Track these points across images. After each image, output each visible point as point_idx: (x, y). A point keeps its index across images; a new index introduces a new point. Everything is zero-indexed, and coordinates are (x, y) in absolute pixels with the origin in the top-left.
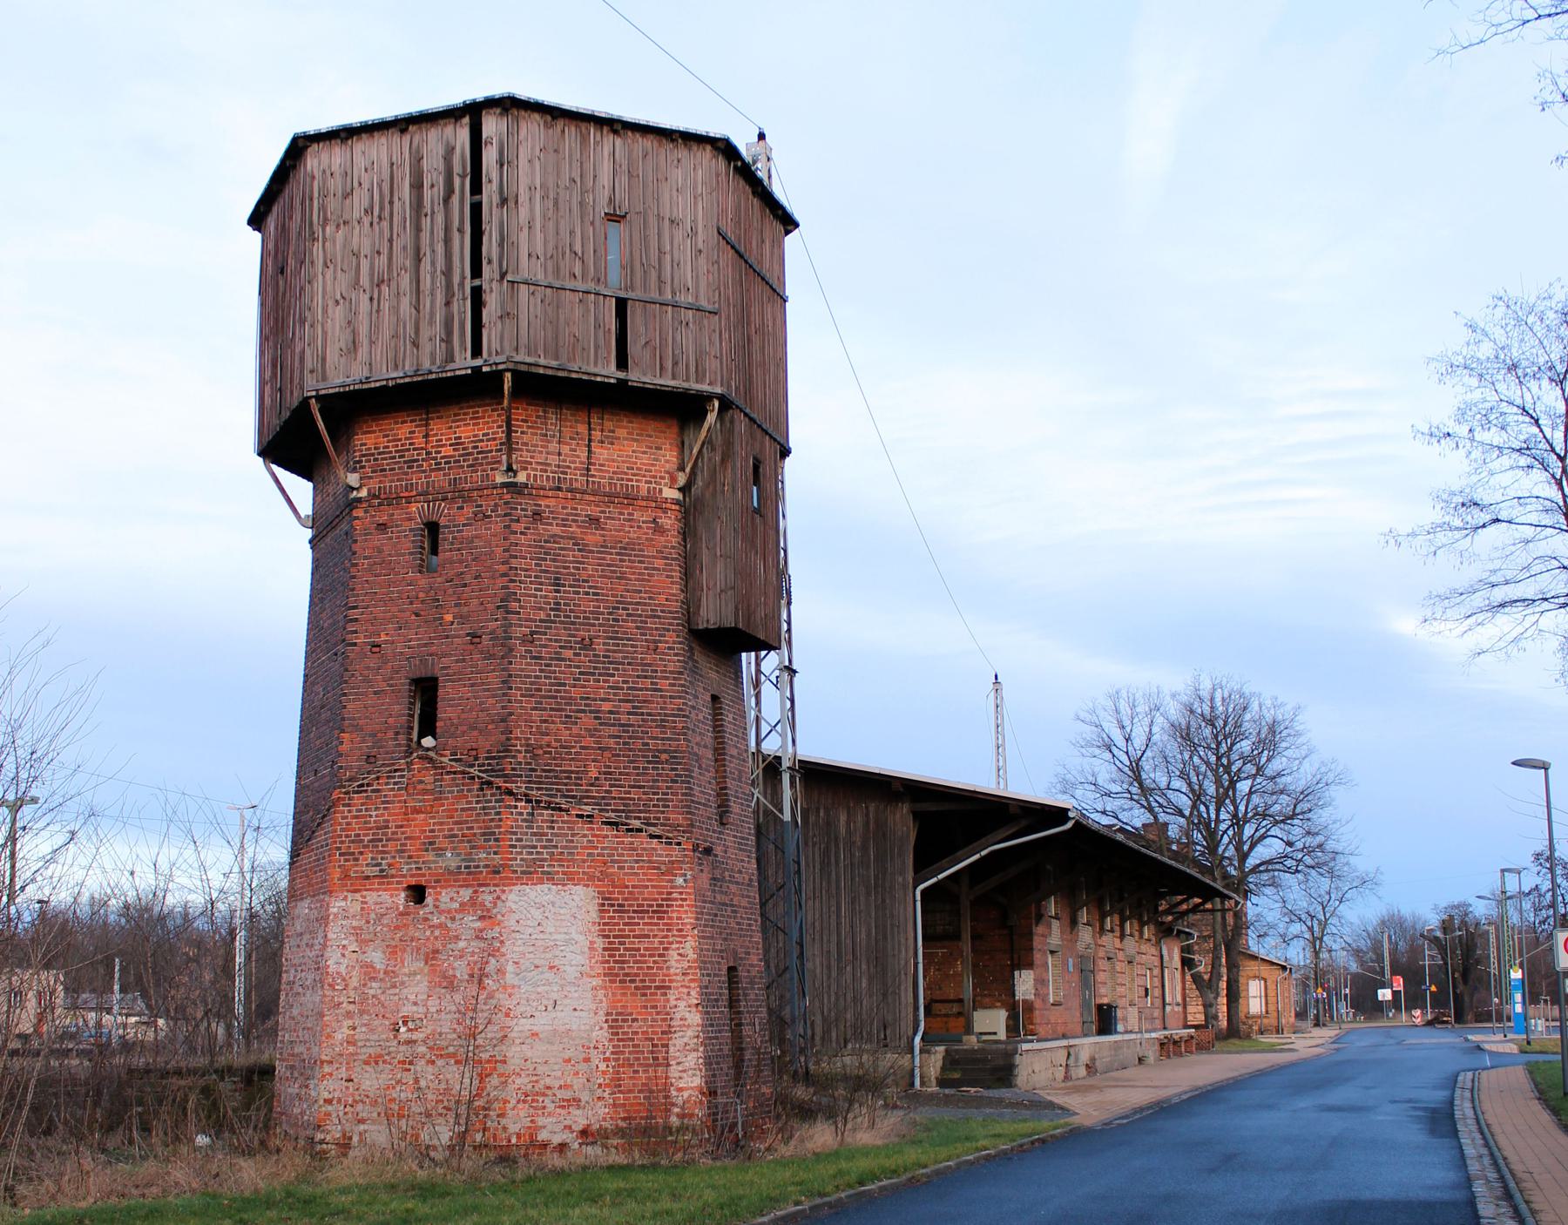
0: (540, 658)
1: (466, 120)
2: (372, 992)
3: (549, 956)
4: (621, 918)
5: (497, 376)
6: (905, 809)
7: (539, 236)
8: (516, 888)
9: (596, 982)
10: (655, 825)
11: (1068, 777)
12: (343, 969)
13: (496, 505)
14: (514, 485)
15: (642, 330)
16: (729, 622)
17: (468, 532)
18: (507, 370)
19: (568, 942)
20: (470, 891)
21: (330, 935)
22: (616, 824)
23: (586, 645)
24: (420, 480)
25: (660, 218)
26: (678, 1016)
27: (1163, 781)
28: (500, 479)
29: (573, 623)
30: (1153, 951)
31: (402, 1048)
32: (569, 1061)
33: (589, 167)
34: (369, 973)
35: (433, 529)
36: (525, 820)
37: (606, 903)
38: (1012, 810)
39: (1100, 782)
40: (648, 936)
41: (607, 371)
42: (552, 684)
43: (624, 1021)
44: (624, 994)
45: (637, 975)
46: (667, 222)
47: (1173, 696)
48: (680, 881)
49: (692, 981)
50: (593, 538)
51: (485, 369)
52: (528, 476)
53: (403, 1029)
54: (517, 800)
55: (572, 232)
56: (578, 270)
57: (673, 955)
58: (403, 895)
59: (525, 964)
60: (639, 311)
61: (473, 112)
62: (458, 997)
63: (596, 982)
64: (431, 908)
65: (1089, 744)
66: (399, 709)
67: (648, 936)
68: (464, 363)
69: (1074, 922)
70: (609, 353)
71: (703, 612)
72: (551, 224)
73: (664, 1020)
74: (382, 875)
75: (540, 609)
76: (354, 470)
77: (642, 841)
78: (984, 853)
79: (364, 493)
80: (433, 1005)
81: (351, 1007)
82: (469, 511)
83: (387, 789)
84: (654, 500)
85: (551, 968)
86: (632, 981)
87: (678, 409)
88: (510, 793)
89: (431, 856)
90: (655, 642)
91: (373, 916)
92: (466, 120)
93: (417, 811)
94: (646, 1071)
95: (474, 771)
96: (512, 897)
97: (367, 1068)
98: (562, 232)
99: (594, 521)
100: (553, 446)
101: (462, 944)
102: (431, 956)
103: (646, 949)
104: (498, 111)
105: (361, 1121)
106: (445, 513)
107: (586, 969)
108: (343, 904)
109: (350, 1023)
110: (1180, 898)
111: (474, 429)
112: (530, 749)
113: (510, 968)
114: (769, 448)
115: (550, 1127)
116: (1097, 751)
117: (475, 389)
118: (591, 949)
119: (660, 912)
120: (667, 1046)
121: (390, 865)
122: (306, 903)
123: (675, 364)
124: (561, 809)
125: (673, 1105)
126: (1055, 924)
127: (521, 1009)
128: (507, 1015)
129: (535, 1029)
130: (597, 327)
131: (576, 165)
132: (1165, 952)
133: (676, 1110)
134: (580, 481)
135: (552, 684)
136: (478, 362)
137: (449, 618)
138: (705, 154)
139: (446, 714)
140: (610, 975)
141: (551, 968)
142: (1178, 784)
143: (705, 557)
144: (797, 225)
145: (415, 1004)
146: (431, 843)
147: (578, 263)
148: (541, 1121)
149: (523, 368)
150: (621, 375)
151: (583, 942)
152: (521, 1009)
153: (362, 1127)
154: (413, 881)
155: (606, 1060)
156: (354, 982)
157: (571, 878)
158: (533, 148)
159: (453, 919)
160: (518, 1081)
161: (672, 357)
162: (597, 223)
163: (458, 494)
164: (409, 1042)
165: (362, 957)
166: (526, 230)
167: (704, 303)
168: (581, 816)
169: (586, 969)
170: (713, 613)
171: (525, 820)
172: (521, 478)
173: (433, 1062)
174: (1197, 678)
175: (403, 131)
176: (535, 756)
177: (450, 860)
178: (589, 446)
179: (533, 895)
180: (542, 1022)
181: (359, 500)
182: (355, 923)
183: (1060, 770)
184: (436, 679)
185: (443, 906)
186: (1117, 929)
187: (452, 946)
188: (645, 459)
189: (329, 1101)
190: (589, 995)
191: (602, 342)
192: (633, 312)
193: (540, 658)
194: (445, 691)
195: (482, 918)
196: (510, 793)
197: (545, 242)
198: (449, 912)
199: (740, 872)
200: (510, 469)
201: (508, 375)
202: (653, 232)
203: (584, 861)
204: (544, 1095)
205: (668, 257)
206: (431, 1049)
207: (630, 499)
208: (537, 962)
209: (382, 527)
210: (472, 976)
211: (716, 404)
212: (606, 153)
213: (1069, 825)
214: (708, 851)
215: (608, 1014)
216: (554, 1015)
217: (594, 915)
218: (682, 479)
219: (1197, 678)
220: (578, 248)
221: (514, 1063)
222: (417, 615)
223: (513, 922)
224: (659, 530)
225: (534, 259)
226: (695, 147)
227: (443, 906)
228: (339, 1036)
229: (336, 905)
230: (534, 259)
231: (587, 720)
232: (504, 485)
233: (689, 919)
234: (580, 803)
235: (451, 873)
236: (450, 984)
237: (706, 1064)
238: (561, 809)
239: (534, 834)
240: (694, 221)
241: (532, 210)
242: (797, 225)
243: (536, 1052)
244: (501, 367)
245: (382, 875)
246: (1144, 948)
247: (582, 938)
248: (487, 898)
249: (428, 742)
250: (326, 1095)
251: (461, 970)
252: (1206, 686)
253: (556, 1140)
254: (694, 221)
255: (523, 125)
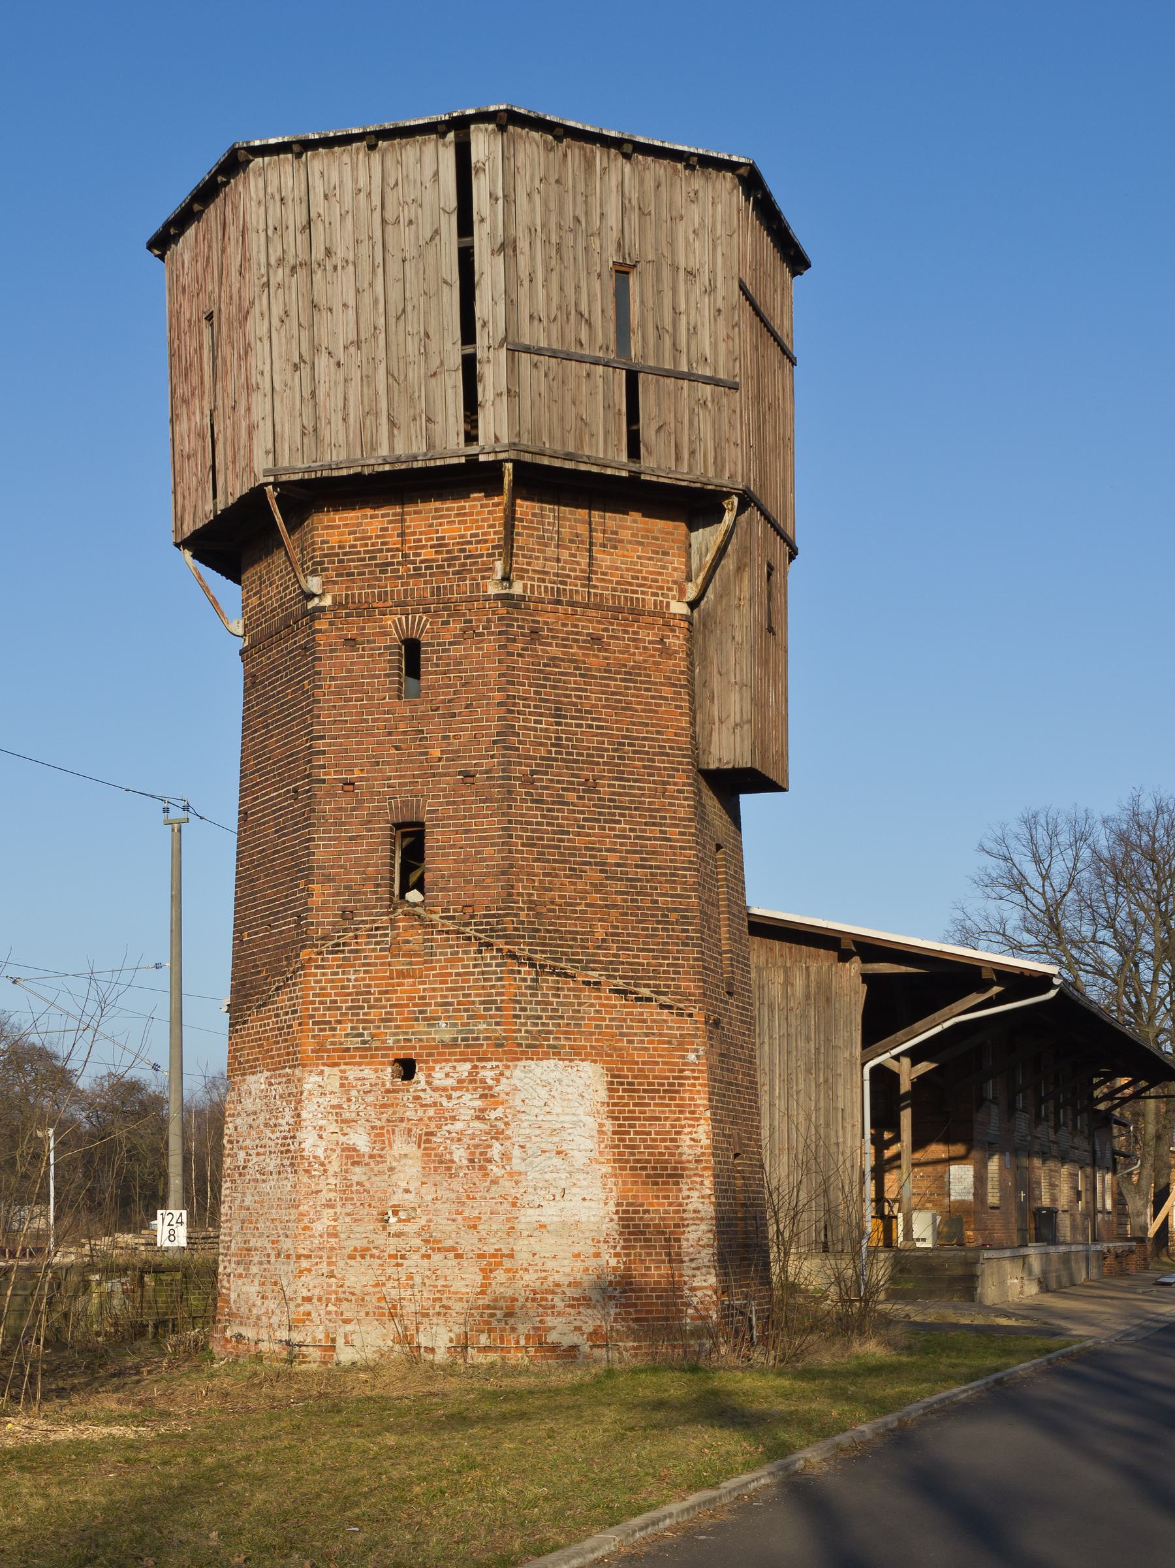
0: (542, 802)
1: (451, 136)
2: (355, 1179)
3: (556, 1139)
4: (632, 1098)
5: (497, 466)
6: (855, 967)
7: (541, 292)
8: (523, 1063)
9: (606, 1169)
10: (665, 994)
11: (968, 923)
12: (320, 1153)
13: (489, 620)
14: (510, 597)
15: (654, 411)
16: (745, 762)
17: (457, 652)
18: (507, 461)
19: (575, 1124)
20: (467, 1066)
21: (304, 1115)
22: (624, 992)
23: (591, 787)
24: (395, 588)
25: (675, 268)
26: (691, 1207)
27: (1087, 930)
28: (493, 590)
29: (576, 761)
30: (1085, 1145)
31: (392, 1241)
32: (578, 1255)
33: (595, 202)
34: (351, 1155)
35: (412, 652)
36: (528, 987)
37: (615, 1080)
38: (985, 975)
39: (1009, 932)
40: (659, 1119)
41: (617, 462)
42: (554, 832)
43: (635, 1212)
44: (635, 1183)
45: (648, 1162)
46: (682, 273)
47: (1105, 822)
48: (692, 1057)
49: (705, 1169)
50: (595, 661)
51: (482, 458)
52: (525, 586)
53: (393, 1220)
54: (520, 964)
55: (577, 288)
56: (584, 338)
57: (686, 1140)
58: (389, 1070)
59: (532, 1148)
60: (652, 388)
61: (461, 125)
62: (456, 1184)
63: (606, 1169)
64: (423, 1085)
65: (993, 883)
66: (379, 855)
67: (659, 1119)
68: (451, 447)
69: (1012, 1108)
70: (619, 440)
71: (714, 749)
72: (555, 277)
73: (678, 1212)
74: (365, 1048)
75: (541, 744)
76: (314, 573)
77: (650, 1012)
78: (947, 1025)
79: (327, 601)
80: (428, 1194)
81: (332, 1195)
82: (456, 627)
83: (369, 949)
84: (660, 613)
85: (558, 1153)
86: (642, 1168)
87: (694, 505)
88: (512, 956)
89: (421, 1026)
90: (665, 783)
91: (354, 1093)
92: (451, 136)
93: (401, 974)
94: (658, 1268)
95: (470, 931)
96: (518, 1073)
97: (352, 1262)
98: (566, 289)
99: (596, 640)
100: (551, 551)
101: (459, 1126)
102: (425, 1139)
103: (657, 1133)
104: (491, 127)
105: (346, 1321)
106: (427, 629)
107: (595, 1154)
108: (318, 1079)
109: (331, 1211)
110: (1124, 1081)
111: (474, 519)
112: (532, 905)
113: (517, 1152)
114: (781, 549)
115: (560, 1327)
116: (1005, 891)
117: (472, 477)
118: (600, 1132)
119: (672, 1092)
120: (678, 1240)
121: (372, 1036)
122: (262, 1077)
123: (692, 453)
124: (566, 975)
125: (688, 1305)
126: (995, 1110)
127: (527, 1198)
128: (514, 1205)
129: (543, 1219)
130: (607, 407)
131: (580, 199)
132: (1098, 1148)
133: (690, 1311)
134: (580, 592)
135: (554, 832)
136: (473, 450)
137: (436, 752)
138: (726, 182)
139: (435, 862)
140: (619, 1160)
141: (558, 1153)
142: (1105, 934)
143: (716, 684)
144: (807, 265)
145: (407, 1191)
146: (421, 1012)
147: (584, 327)
148: (550, 1321)
149: (527, 458)
150: (634, 467)
151: (592, 1123)
152: (527, 1198)
153: (349, 1328)
154: (402, 1054)
155: (617, 1255)
156: (334, 1167)
157: (577, 1054)
158: (532, 180)
159: (450, 1098)
160: (527, 1277)
161: (691, 442)
162: (605, 275)
163: (442, 606)
164: (398, 1235)
165: (342, 1139)
166: (526, 283)
167: (722, 375)
168: (588, 983)
169: (595, 1154)
170: (728, 750)
171: (528, 987)
172: (517, 588)
173: (429, 1257)
174: (1136, 801)
175: (372, 147)
176: (538, 915)
177: (444, 1031)
178: (590, 551)
179: (538, 1071)
180: (550, 1213)
181: (322, 609)
182: (335, 1102)
183: (958, 915)
184: (422, 824)
185: (436, 1083)
186: (1052, 1116)
187: (449, 1127)
188: (651, 566)
189: (308, 1300)
190: (598, 1182)
191: (612, 428)
192: (646, 391)
193: (542, 802)
194: (434, 839)
195: (483, 1096)
196: (512, 956)
197: (549, 299)
198: (445, 1089)
199: (742, 1047)
200: (506, 578)
201: (509, 466)
202: (666, 286)
203: (592, 1034)
204: (554, 1293)
205: (683, 318)
206: (426, 1241)
207: (637, 613)
208: (543, 1146)
209: (351, 642)
210: (472, 1161)
211: (735, 500)
212: (614, 183)
213: (1052, 993)
214: (717, 1023)
215: (618, 1205)
216: (562, 1204)
217: (603, 1095)
218: (692, 592)
219: (1136, 801)
220: (584, 308)
221: (523, 1257)
222: (397, 748)
223: (518, 1102)
224: (666, 652)
225: (536, 322)
226: (713, 173)
227: (436, 1083)
228: (319, 1227)
229: (311, 1081)
230: (536, 322)
231: (592, 874)
232: (498, 597)
233: (702, 1100)
234: (586, 968)
235: (445, 1046)
236: (446, 1166)
237: (719, 1261)
238: (566, 975)
239: (538, 1003)
240: (713, 272)
241: (533, 258)
242: (807, 265)
243: (547, 1245)
244: (502, 456)
245: (365, 1048)
246: (1078, 1141)
247: (591, 1119)
248: (488, 1074)
249: (414, 896)
250: (305, 1293)
251: (460, 1154)
252: (1147, 805)
253: (566, 1341)
254: (713, 272)
255: (520, 146)
